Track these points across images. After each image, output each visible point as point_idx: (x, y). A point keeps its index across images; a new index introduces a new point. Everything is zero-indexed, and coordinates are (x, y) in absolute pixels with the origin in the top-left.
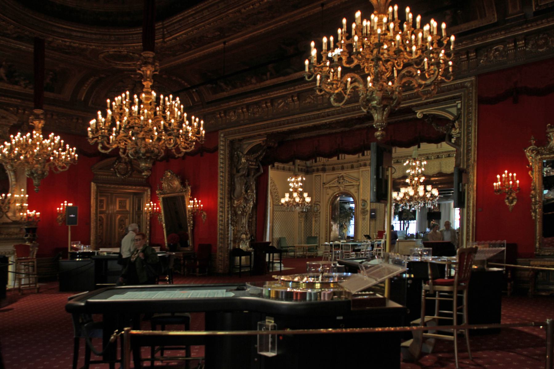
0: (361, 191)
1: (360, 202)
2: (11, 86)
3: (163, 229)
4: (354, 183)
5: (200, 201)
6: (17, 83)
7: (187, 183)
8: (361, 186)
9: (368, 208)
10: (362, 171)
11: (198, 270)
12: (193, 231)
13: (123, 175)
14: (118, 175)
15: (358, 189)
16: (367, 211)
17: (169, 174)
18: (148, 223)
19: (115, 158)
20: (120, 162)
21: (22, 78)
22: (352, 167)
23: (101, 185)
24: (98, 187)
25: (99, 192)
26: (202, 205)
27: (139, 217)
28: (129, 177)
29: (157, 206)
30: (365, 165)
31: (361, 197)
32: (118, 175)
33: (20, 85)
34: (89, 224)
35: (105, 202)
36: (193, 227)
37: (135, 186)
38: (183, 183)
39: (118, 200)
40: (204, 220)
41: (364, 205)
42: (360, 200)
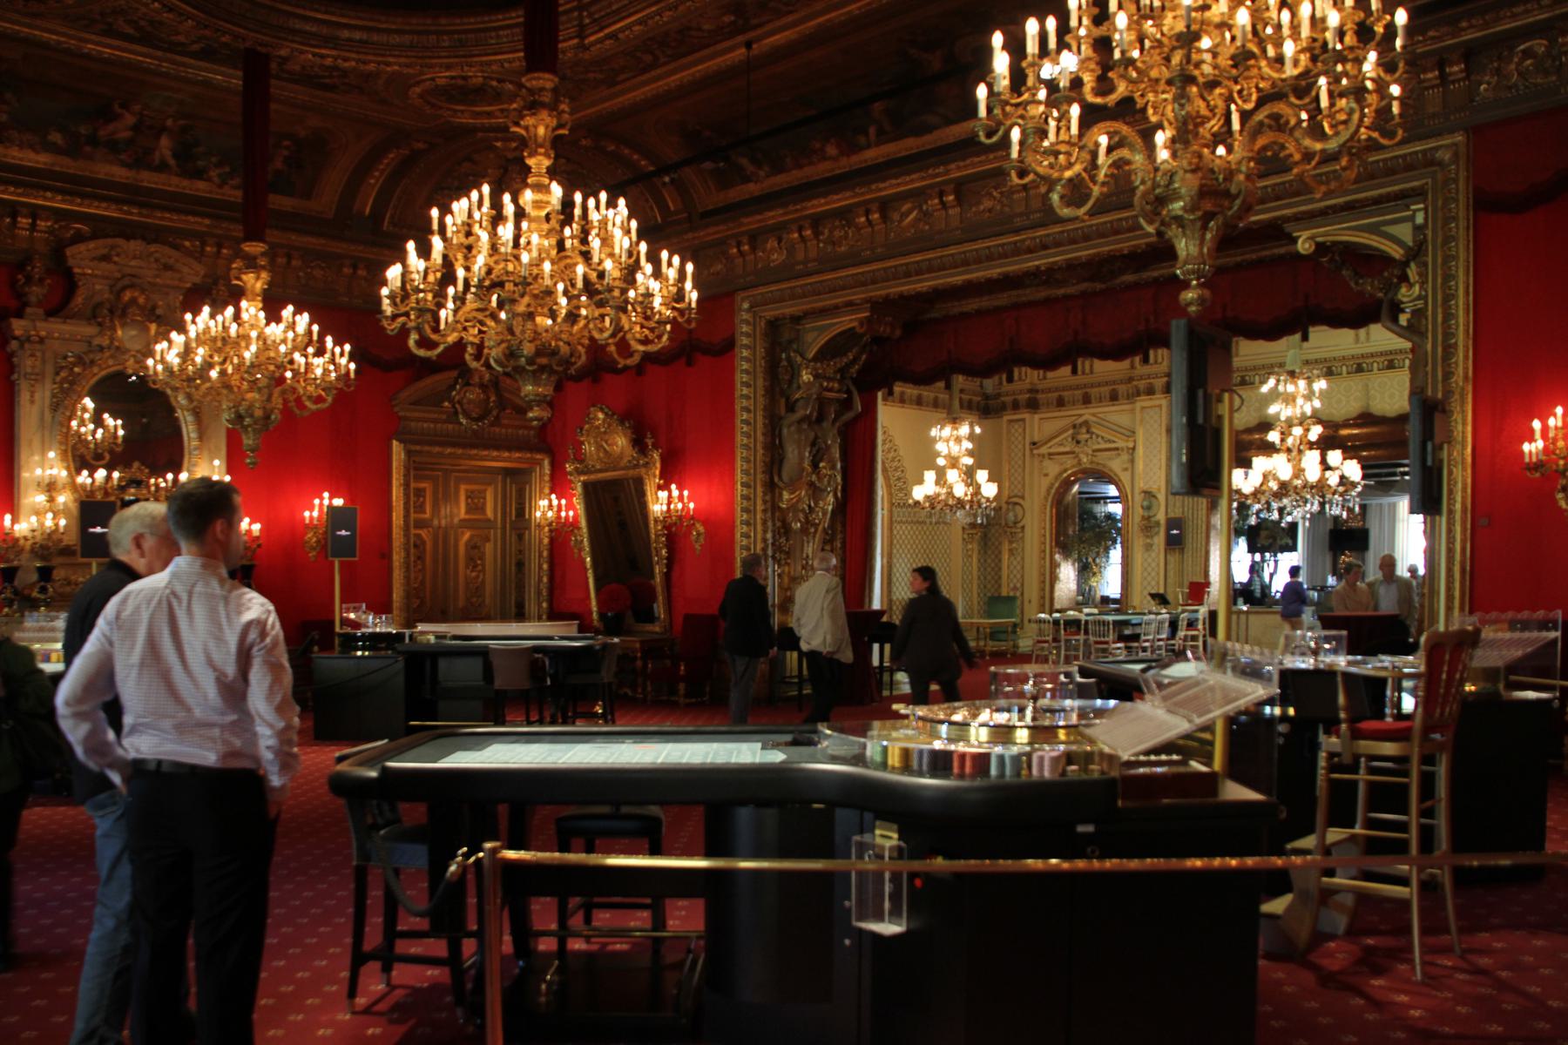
0: (1140, 465)
1: (1138, 498)
2: (185, 183)
3: (586, 570)
4: (1120, 444)
5: (686, 493)
6: (199, 174)
7: (649, 442)
8: (1140, 451)
9: (1161, 517)
10: (1143, 408)
11: (682, 687)
12: (667, 576)
13: (480, 418)
14: (464, 421)
15: (1132, 461)
16: (1158, 523)
17: (601, 416)
18: (545, 554)
19: (455, 373)
20: (468, 384)
21: (214, 160)
22: (1114, 397)
23: (418, 448)
24: (409, 453)
25: (415, 468)
26: (692, 505)
27: (520, 537)
28: (492, 425)
29: (570, 506)
30: (1150, 391)
31: (1141, 484)
32: (464, 421)
33: (209, 180)
34: (386, 555)
35: (428, 494)
36: (669, 566)
37: (509, 449)
38: (638, 443)
39: (463, 488)
40: (697, 547)
41: (1149, 508)
42: (1137, 491)
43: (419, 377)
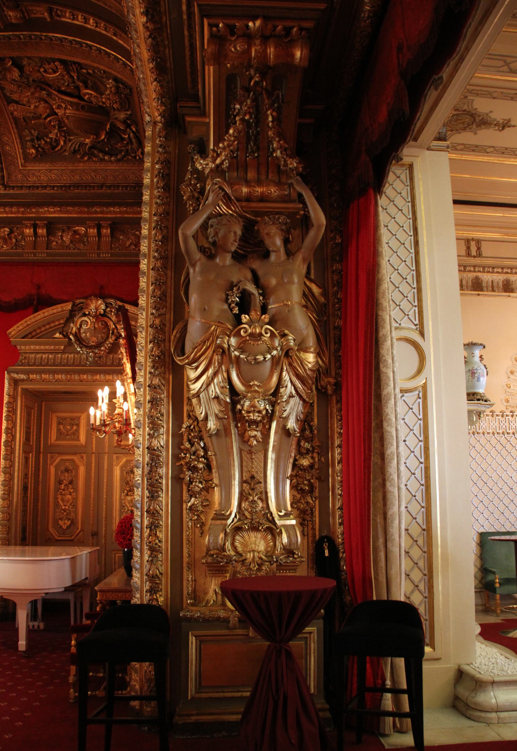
19: (69, 306)
43: (36, 311)
